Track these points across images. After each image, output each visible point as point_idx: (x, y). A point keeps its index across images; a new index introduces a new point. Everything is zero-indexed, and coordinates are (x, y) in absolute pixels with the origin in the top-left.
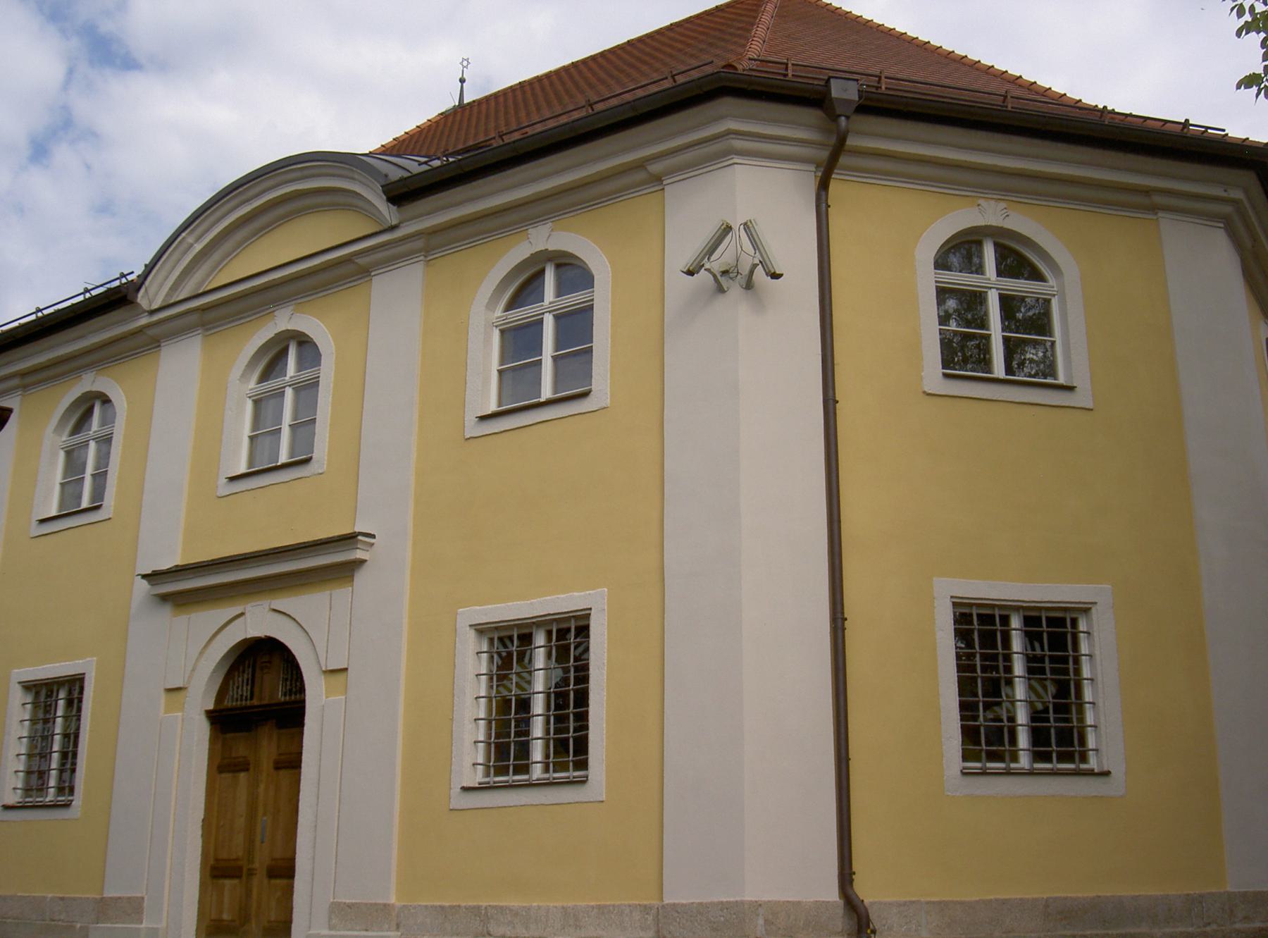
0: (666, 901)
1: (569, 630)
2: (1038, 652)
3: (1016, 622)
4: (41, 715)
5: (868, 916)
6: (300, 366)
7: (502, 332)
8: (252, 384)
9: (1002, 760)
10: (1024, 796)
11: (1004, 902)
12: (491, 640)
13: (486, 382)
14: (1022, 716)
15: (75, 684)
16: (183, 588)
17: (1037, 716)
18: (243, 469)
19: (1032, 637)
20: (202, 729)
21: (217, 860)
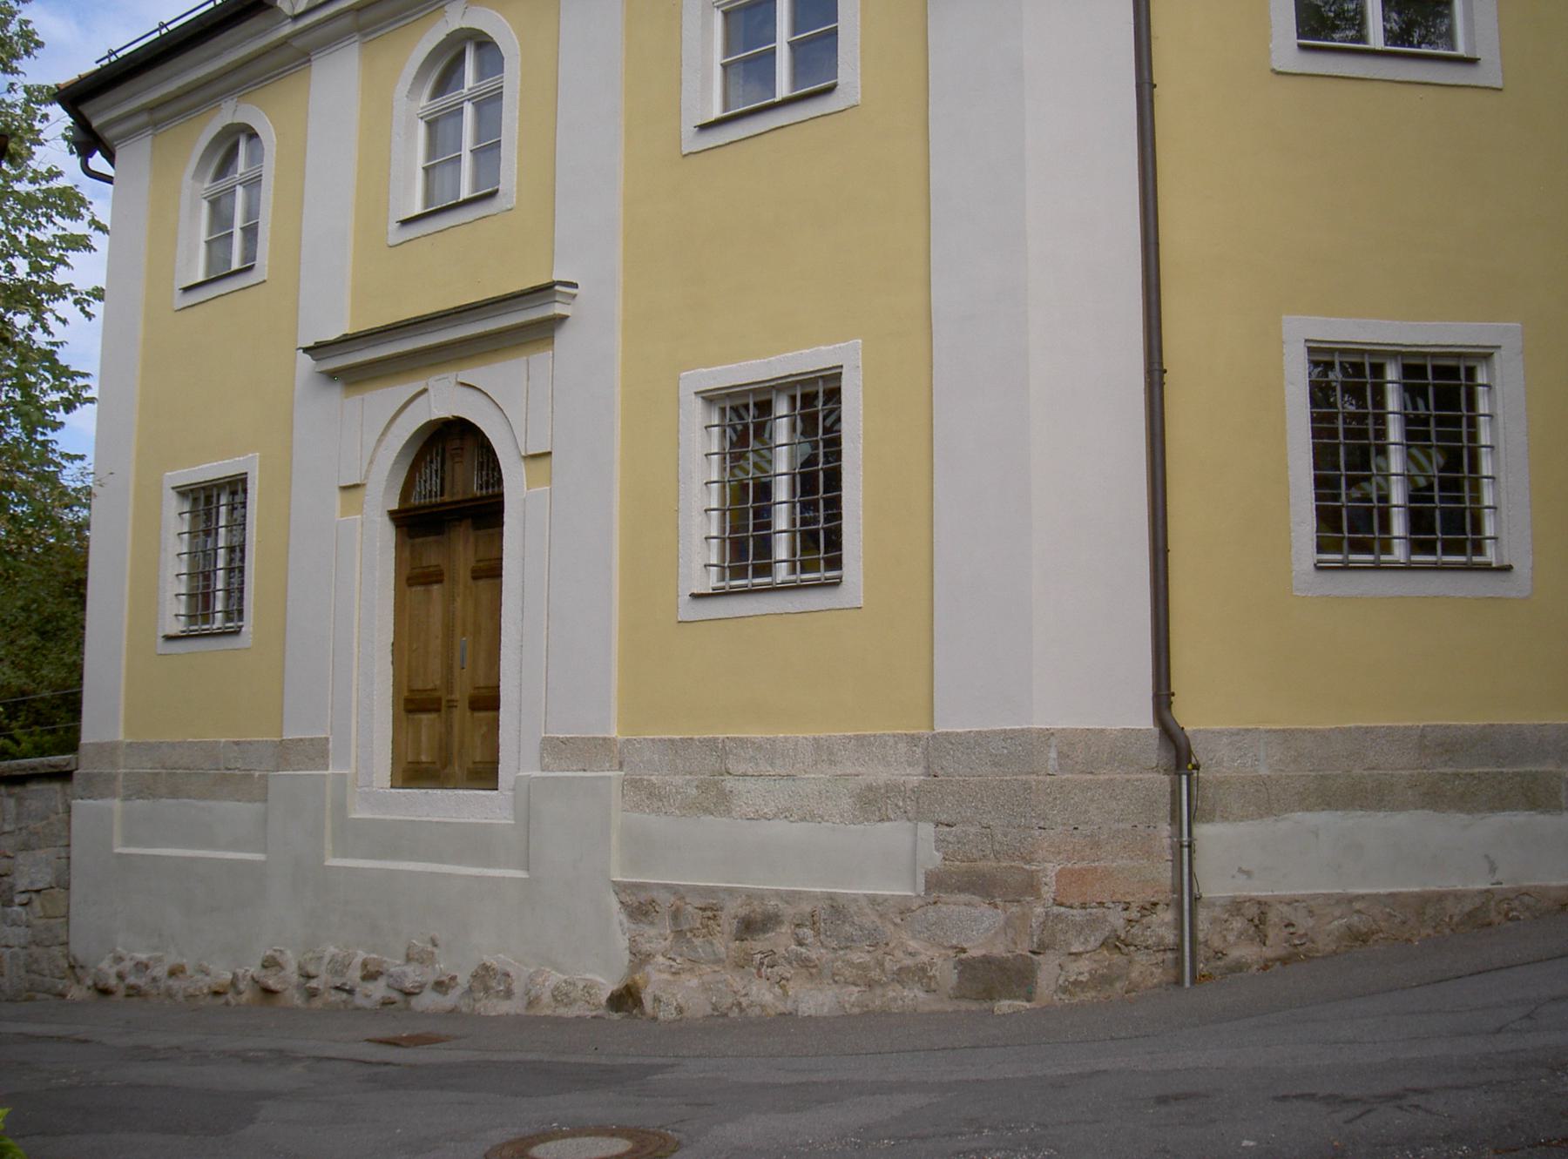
0: (939, 729)
2: (1422, 411)
3: (1392, 373)
4: (202, 527)
5: (1189, 746)
6: (481, 74)
7: (726, 14)
8: (424, 101)
9: (1370, 551)
10: (1400, 597)
11: (1368, 731)
12: (723, 410)
13: (707, 79)
14: (1397, 495)
15: (236, 486)
16: (353, 362)
17: (1417, 495)
18: (418, 209)
19: (1413, 392)
20: (386, 534)
21: (411, 691)
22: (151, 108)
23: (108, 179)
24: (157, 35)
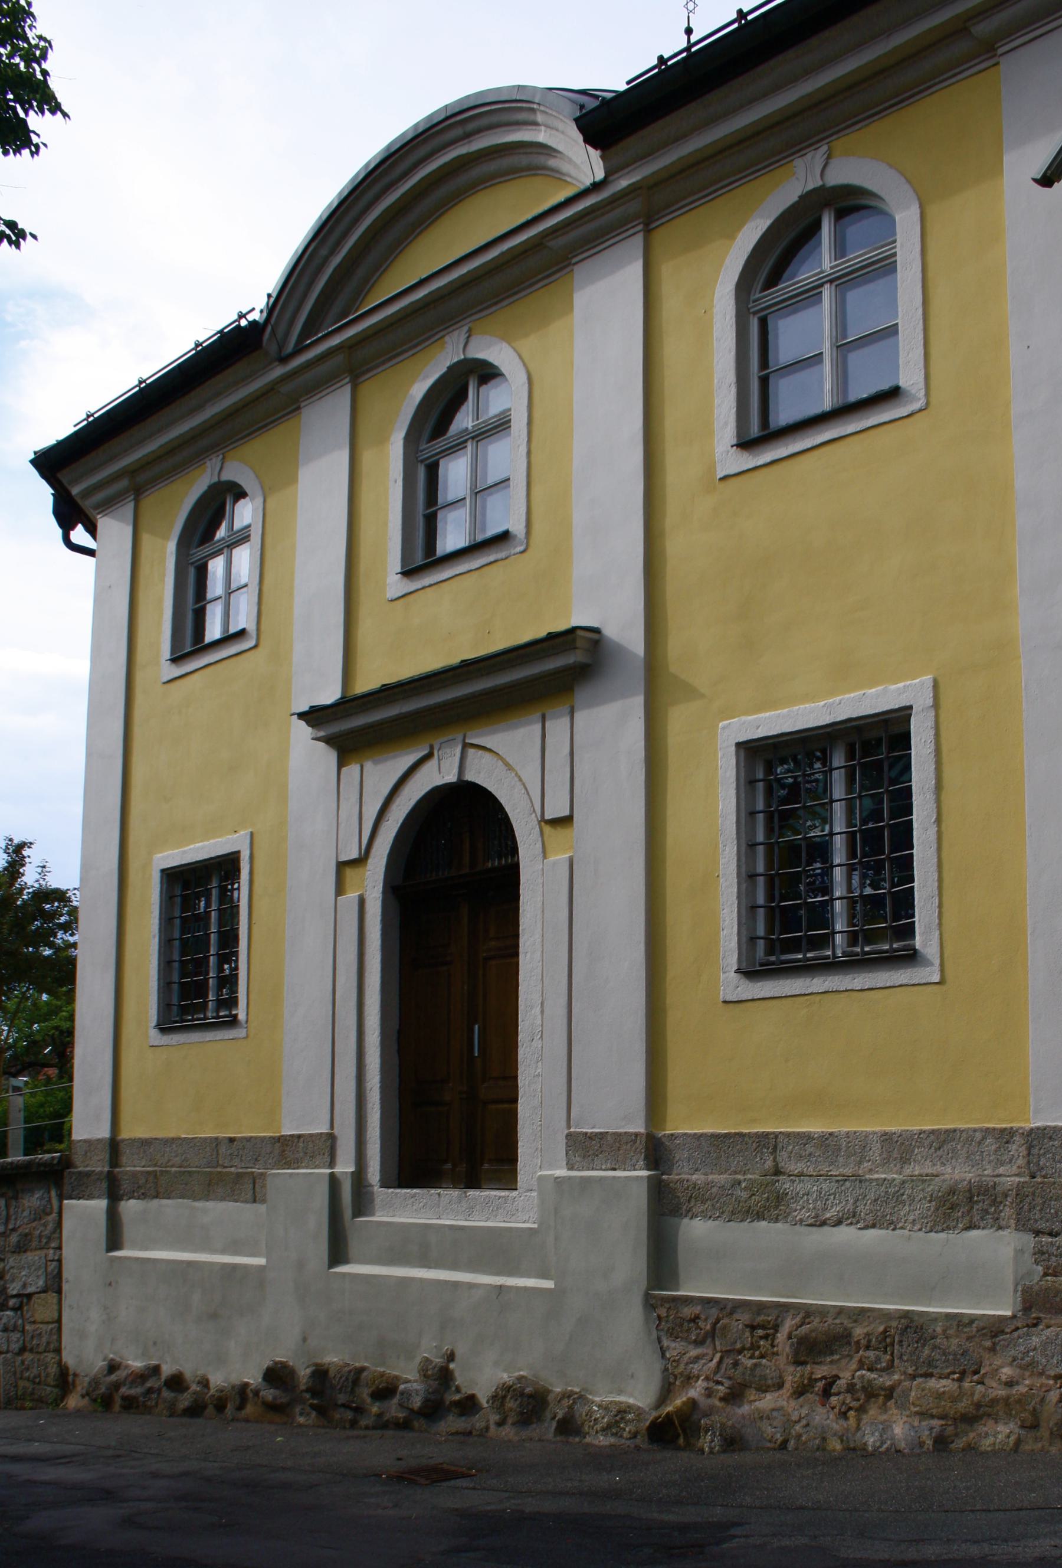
1: (879, 741)
16: (354, 726)
22: (131, 472)
23: (91, 553)
24: (85, 423)
